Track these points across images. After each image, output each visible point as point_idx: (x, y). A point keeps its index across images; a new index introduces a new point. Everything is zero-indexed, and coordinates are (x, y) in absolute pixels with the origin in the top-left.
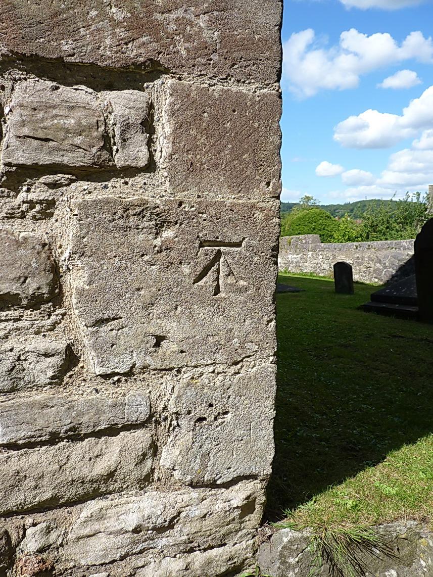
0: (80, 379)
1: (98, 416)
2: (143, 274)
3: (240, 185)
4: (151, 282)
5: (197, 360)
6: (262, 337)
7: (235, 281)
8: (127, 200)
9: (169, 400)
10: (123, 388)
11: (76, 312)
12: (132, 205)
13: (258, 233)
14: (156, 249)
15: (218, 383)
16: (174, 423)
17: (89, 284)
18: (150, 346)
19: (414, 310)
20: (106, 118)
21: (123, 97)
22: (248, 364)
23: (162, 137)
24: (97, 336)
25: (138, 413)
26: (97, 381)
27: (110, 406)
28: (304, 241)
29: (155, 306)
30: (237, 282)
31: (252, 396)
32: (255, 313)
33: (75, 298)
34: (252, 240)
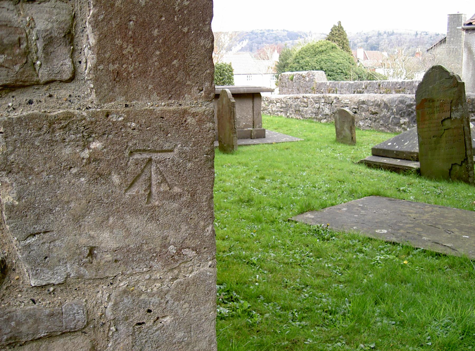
0: (17, 290)
1: (36, 325)
2: (72, 187)
3: (170, 92)
4: (80, 195)
5: (133, 269)
6: (199, 242)
7: (168, 188)
8: (52, 114)
9: (106, 308)
10: (60, 298)
11: (8, 227)
12: (58, 119)
13: (191, 139)
14: (85, 161)
15: (155, 289)
16: (113, 328)
17: (19, 200)
18: (84, 257)
19: (415, 167)
20: (28, 34)
21: (45, 11)
22: (186, 269)
23: (87, 48)
24: (30, 250)
25: (75, 321)
26: (34, 292)
27: (48, 315)
28: (307, 79)
29: (86, 218)
30: (170, 189)
31: (191, 300)
32: (191, 219)
33: (5, 215)
34: (185, 146)
